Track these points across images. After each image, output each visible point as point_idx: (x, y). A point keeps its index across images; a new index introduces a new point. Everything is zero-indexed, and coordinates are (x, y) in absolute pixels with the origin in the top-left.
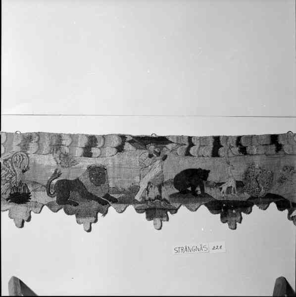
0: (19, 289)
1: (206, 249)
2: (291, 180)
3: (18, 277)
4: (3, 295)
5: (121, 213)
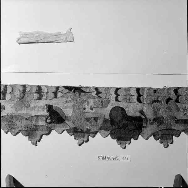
0: (12, 182)
4: (2, 186)
5: (15, 135)
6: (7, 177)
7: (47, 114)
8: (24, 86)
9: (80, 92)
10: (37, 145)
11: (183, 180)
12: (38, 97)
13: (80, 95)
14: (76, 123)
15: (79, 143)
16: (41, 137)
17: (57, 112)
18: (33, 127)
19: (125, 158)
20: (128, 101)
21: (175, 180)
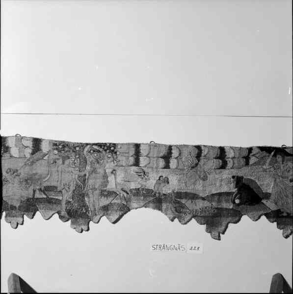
0: (18, 286)
1: (184, 249)
2: (13, 182)
3: (17, 274)
4: (2, 292)
6: (10, 278)
7: (235, 190)
8: (198, 147)
9: (283, 155)
10: (220, 239)
11: (285, 282)
12: (221, 164)
13: (283, 161)
14: (280, 203)
15: (286, 234)
16: (227, 227)
17: (250, 187)
18: (214, 211)
19: (195, 247)
20: (155, 170)
21: (272, 282)
